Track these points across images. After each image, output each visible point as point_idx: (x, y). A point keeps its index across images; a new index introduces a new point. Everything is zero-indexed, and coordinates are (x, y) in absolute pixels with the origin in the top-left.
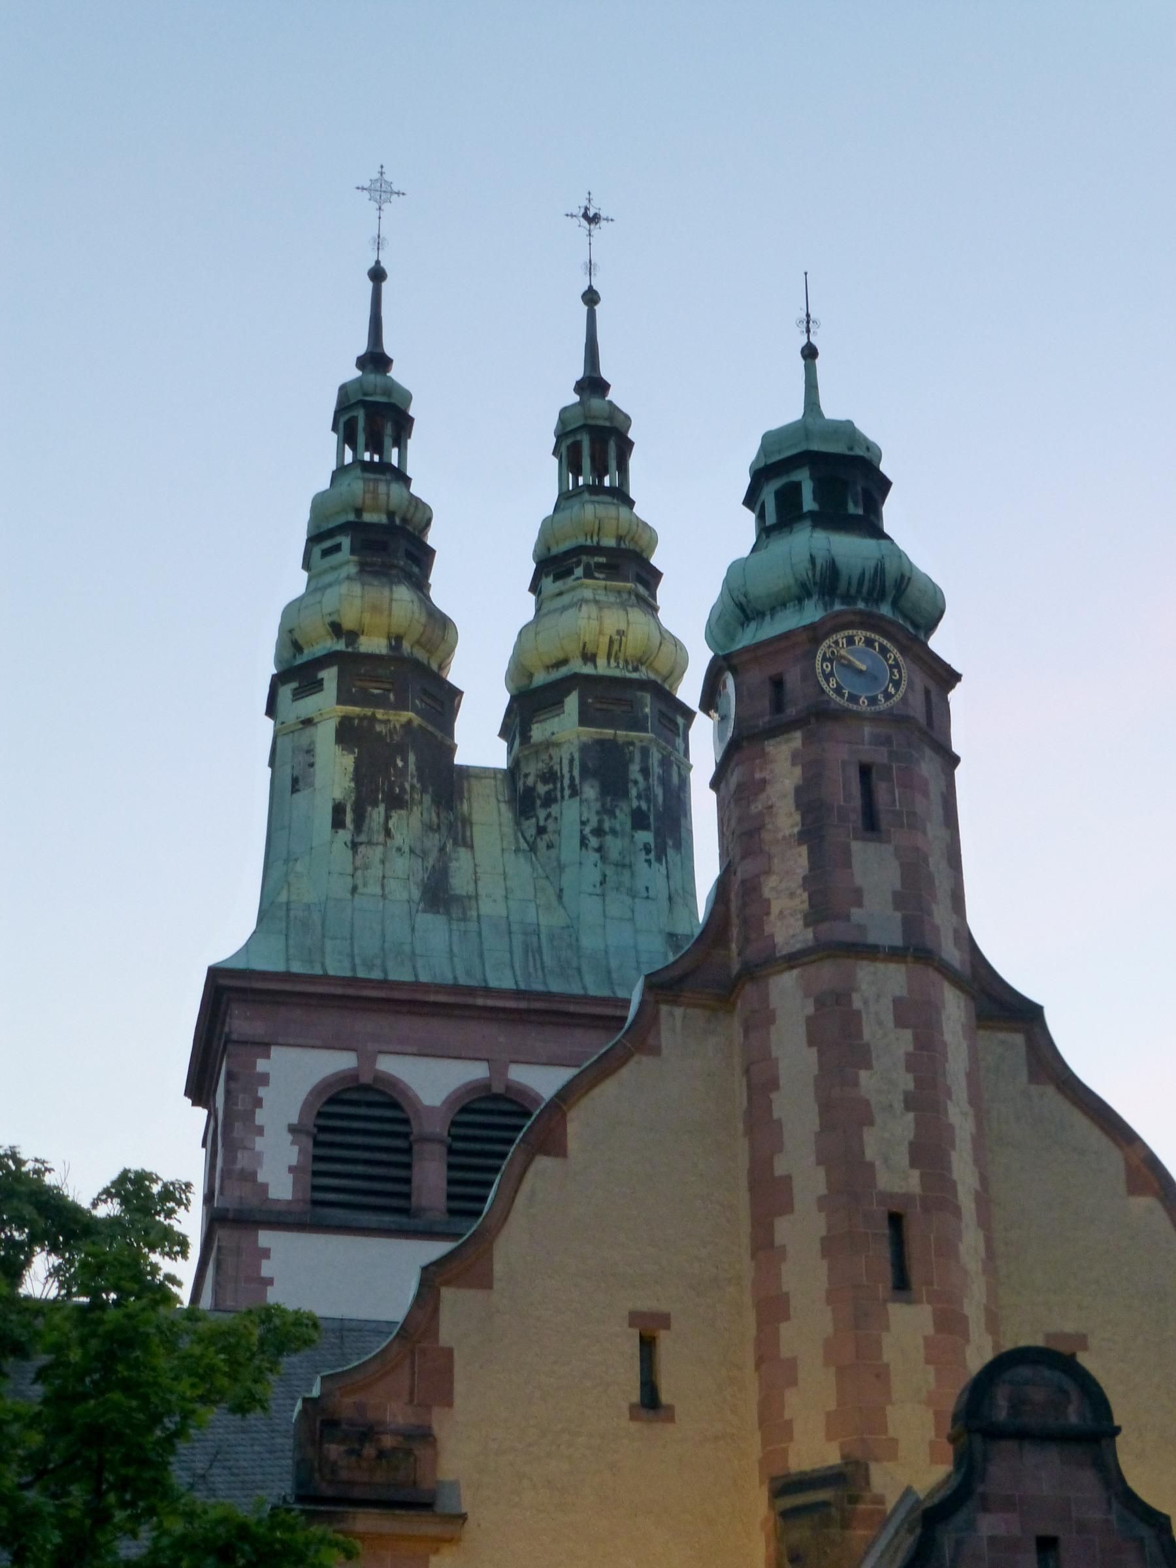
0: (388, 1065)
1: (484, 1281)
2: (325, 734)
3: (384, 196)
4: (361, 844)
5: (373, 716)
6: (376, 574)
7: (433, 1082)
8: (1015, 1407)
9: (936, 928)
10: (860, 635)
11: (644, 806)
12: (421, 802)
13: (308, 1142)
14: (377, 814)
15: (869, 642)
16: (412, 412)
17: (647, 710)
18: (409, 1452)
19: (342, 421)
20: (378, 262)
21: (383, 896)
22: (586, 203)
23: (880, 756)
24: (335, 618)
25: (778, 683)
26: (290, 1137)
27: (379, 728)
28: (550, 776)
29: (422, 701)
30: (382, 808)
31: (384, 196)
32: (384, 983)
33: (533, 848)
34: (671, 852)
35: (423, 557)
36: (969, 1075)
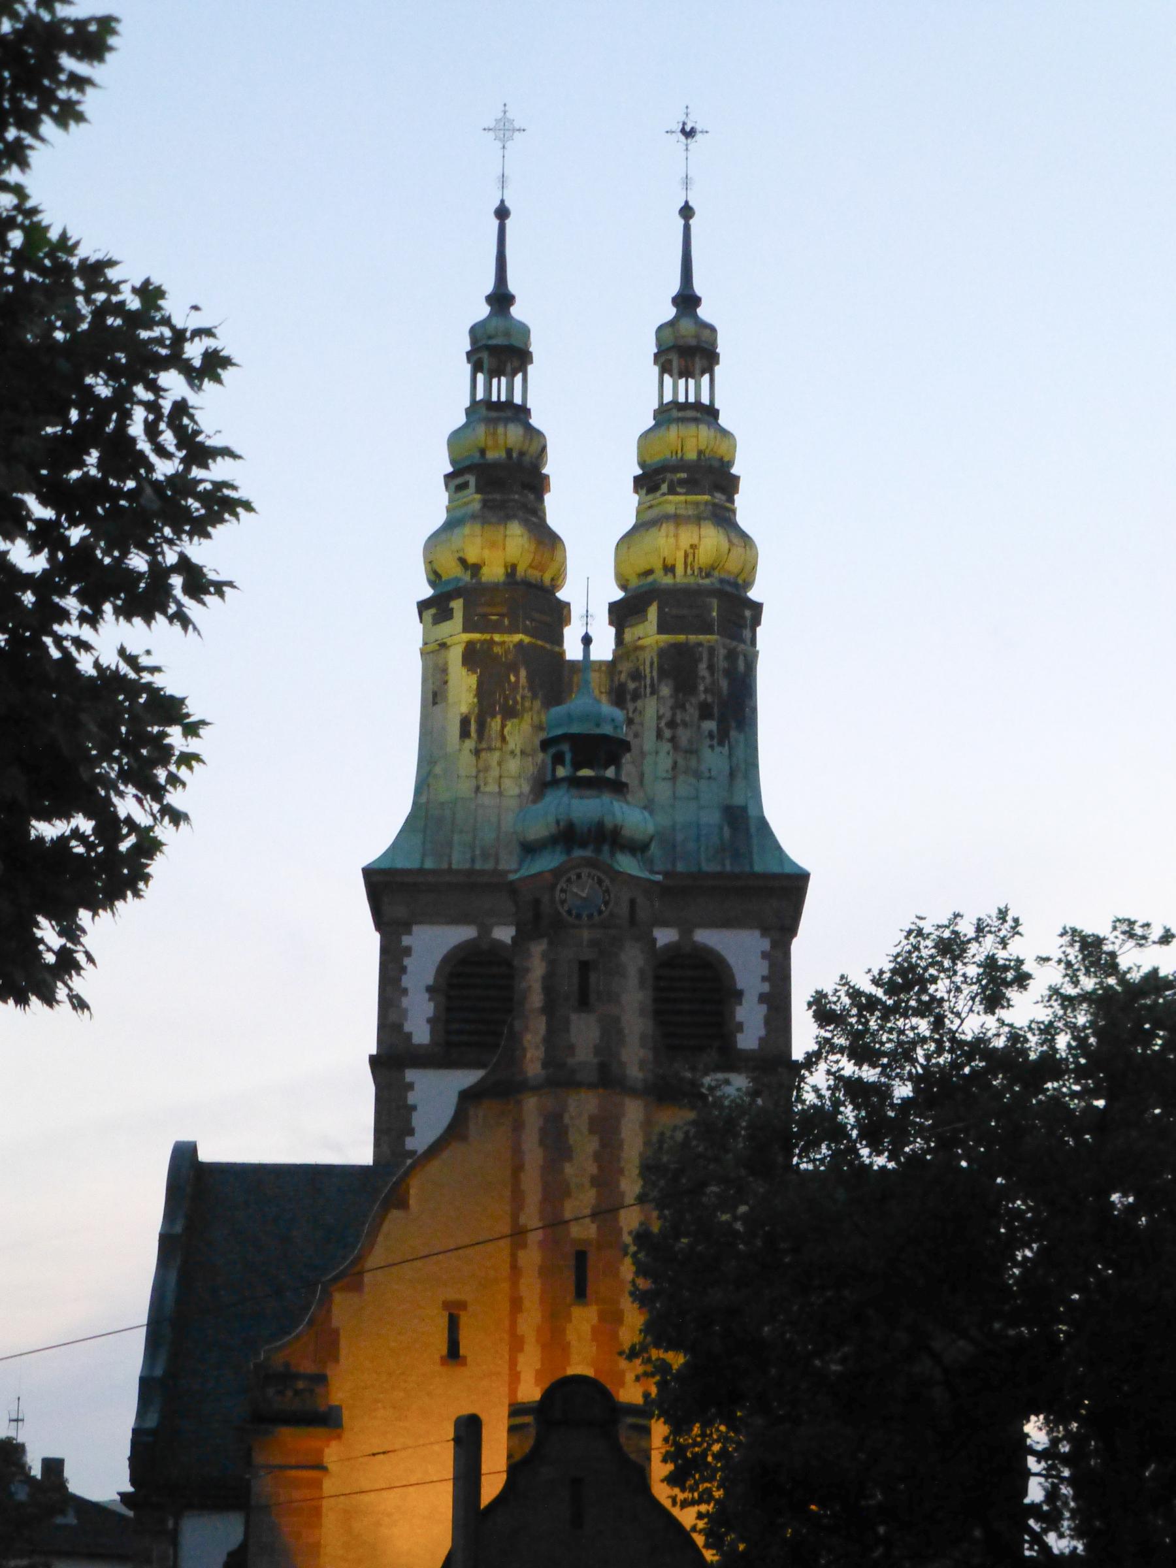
2: (455, 655)
3: (508, 134)
4: (483, 749)
5: (492, 640)
11: (709, 699)
12: (531, 709)
14: (495, 724)
16: (531, 349)
17: (715, 614)
18: (312, 1391)
20: (502, 201)
21: (500, 793)
22: (683, 118)
24: (461, 554)
26: (427, 996)
27: (497, 650)
28: (636, 675)
29: (532, 620)
30: (498, 719)
31: (508, 134)
34: (733, 734)
35: (537, 484)
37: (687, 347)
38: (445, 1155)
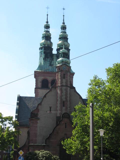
0: (47, 77)
1: (41, 105)
14: (46, 59)
25: (59, 68)
35: (50, 38)
36: (69, 93)
38: (50, 93)
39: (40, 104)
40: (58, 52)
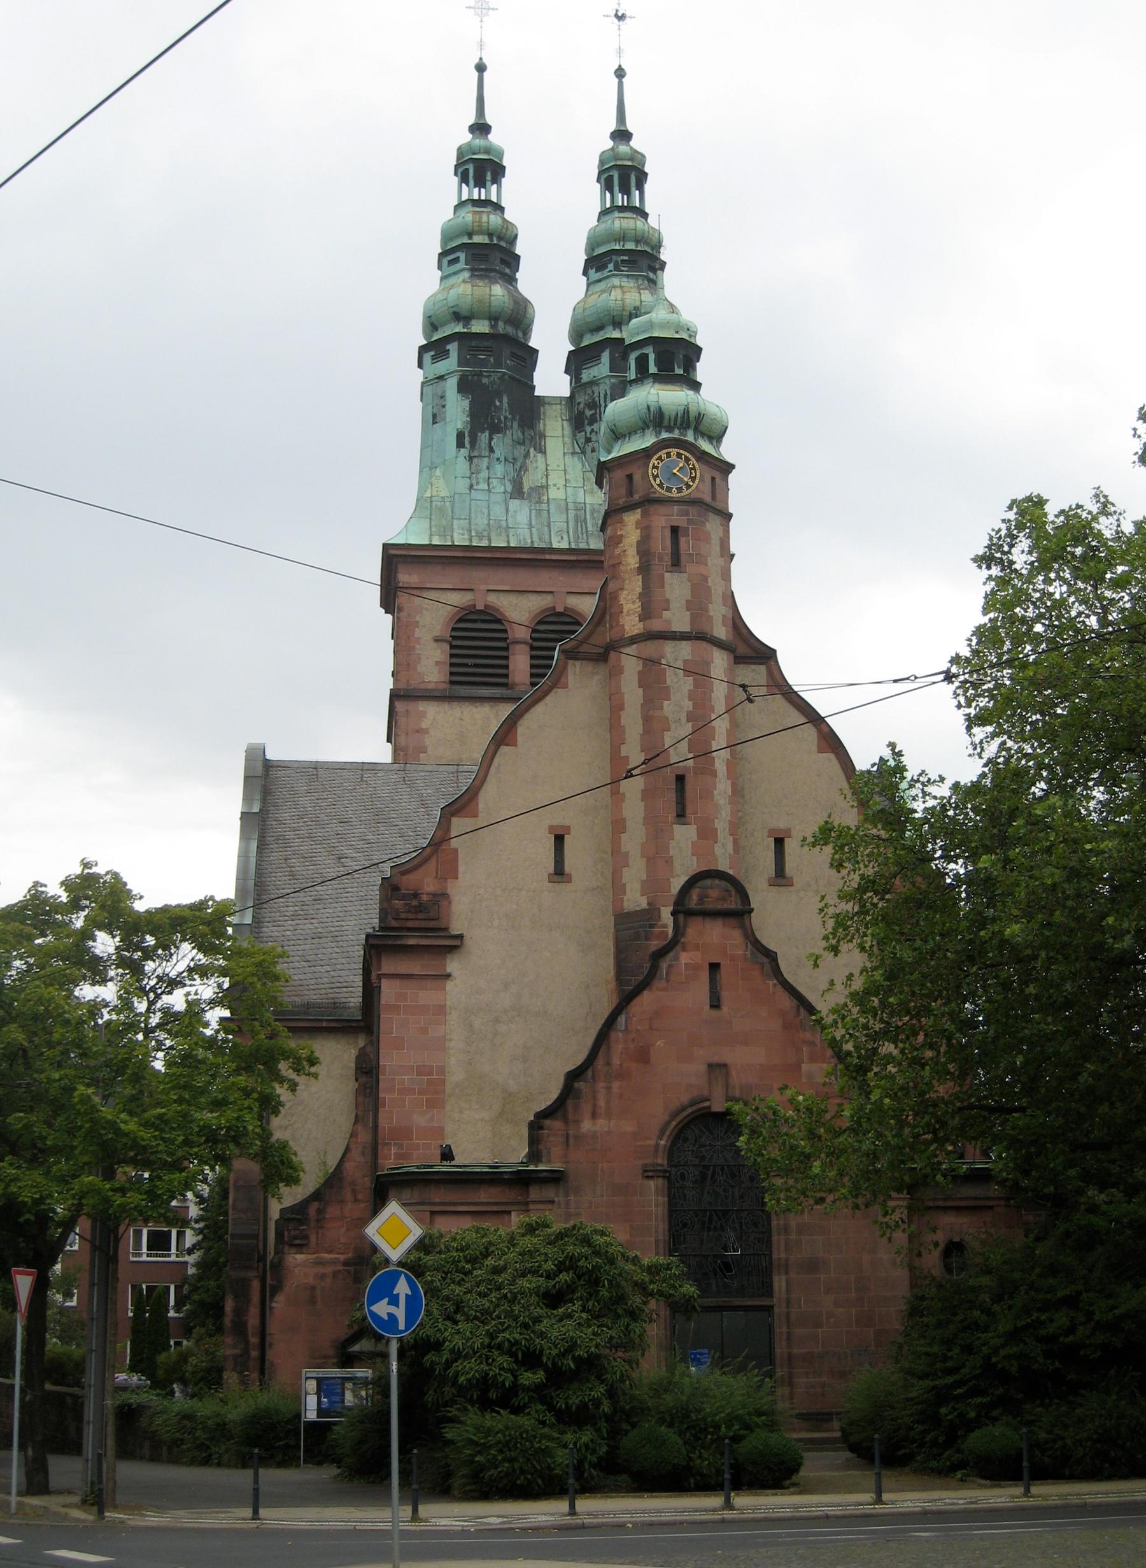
0: (492, 599)
2: (452, 383)
6: (480, 277)
7: (520, 610)
8: (701, 899)
9: (710, 618)
10: (674, 451)
13: (447, 647)
14: (484, 437)
15: (679, 455)
19: (460, 171)
22: (616, 7)
23: (681, 522)
25: (630, 477)
30: (487, 434)
32: (489, 548)
33: (583, 452)
35: (512, 261)
37: (623, 174)
39: (462, 804)
40: (578, 385)
